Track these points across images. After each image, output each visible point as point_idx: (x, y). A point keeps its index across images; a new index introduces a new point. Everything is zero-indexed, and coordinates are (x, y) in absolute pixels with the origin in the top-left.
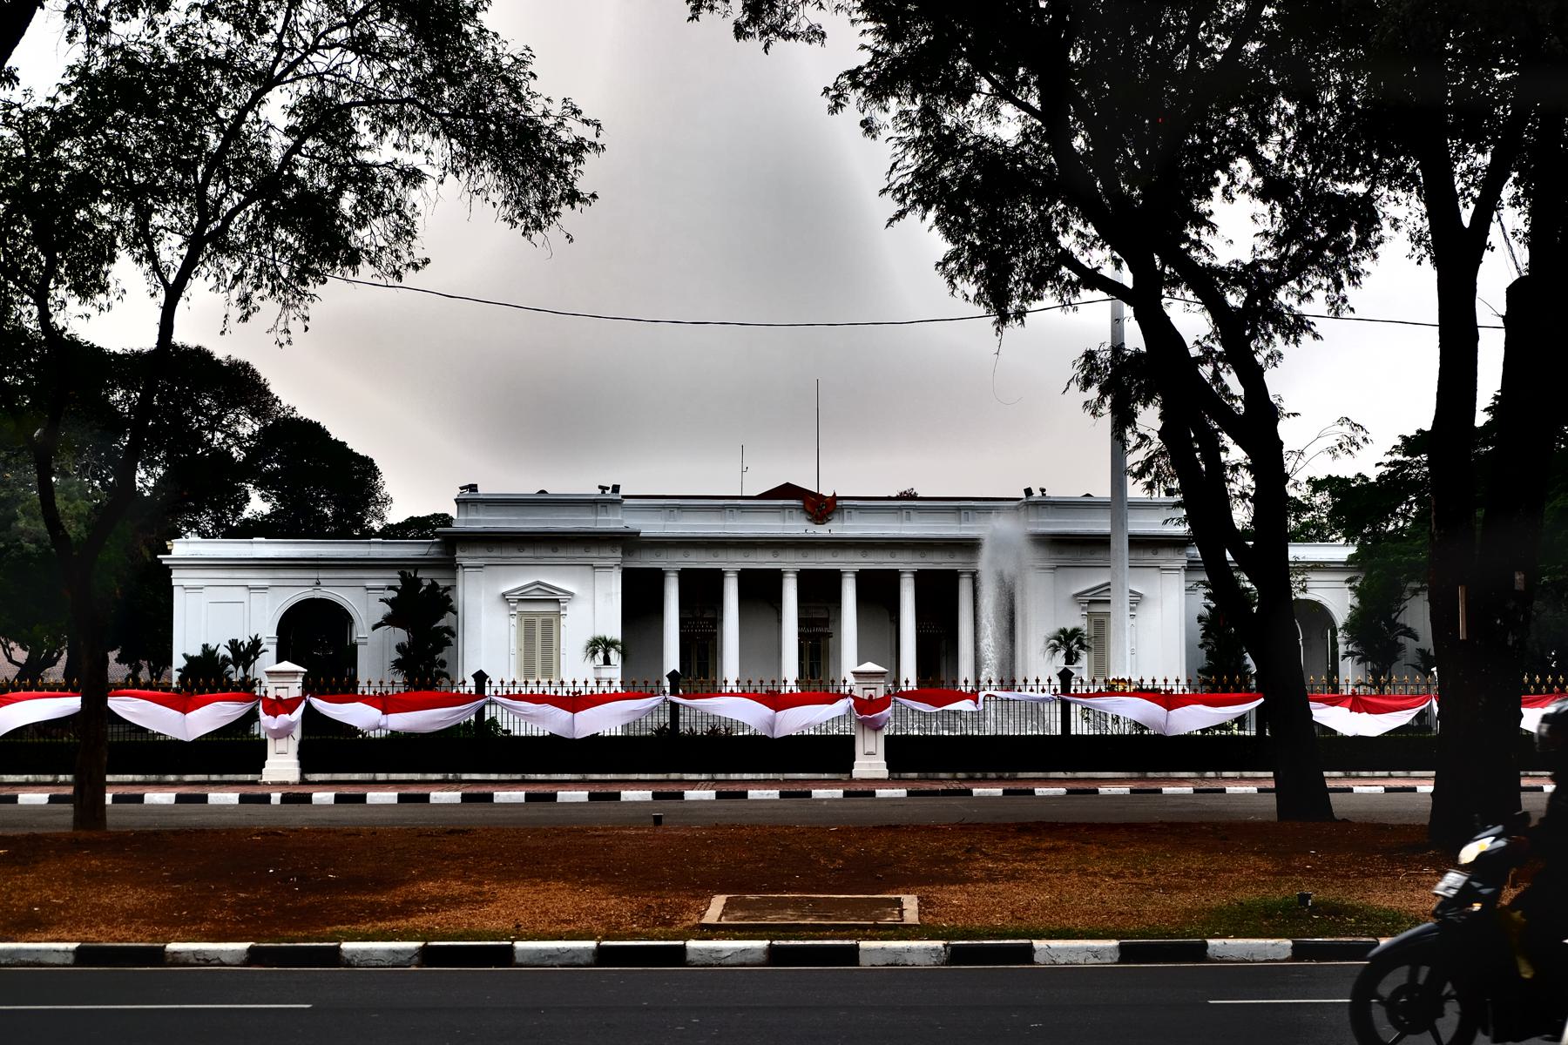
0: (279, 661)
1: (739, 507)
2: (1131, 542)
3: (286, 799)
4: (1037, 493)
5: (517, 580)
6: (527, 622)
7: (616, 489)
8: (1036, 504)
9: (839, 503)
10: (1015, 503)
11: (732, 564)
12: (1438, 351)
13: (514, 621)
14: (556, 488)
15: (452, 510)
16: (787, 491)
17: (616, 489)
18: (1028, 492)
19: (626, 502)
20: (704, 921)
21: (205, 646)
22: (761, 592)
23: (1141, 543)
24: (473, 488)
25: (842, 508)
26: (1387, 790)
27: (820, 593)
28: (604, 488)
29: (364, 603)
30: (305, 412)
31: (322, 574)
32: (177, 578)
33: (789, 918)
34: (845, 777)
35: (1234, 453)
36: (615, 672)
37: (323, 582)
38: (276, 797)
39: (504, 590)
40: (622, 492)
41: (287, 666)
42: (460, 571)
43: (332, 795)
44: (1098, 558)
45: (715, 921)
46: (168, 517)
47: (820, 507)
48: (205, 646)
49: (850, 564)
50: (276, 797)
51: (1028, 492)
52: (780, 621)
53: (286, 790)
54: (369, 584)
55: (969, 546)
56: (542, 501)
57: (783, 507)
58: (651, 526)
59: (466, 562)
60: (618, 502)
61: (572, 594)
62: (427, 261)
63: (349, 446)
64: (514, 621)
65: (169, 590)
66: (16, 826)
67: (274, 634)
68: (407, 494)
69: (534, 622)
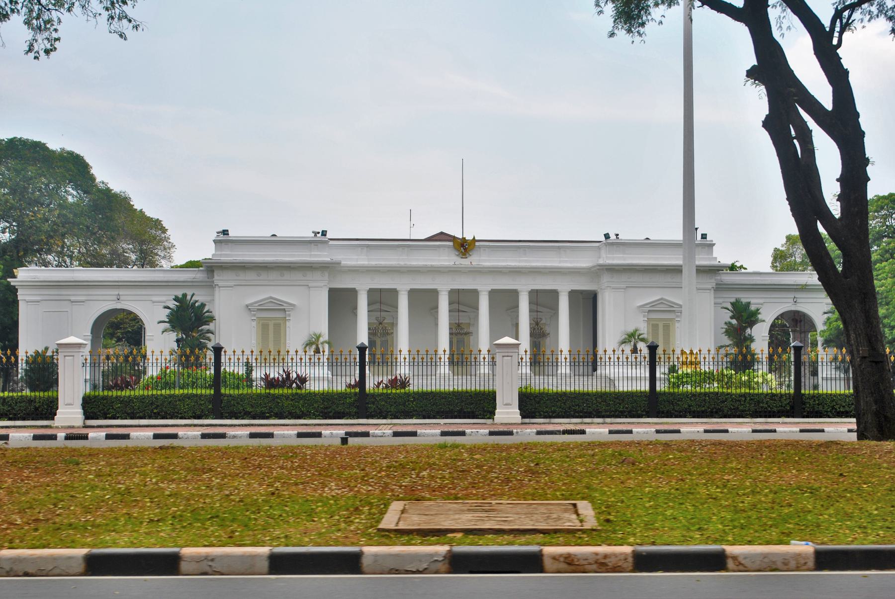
1: (409, 246)
2: (681, 271)
4: (613, 237)
5: (257, 295)
6: (263, 325)
7: (324, 233)
8: (612, 244)
9: (477, 244)
10: (597, 244)
11: (403, 286)
12: (793, 219)
13: (254, 324)
14: (283, 233)
16: (441, 237)
17: (324, 233)
18: (607, 236)
19: (331, 242)
20: (381, 526)
22: (425, 301)
24: (225, 232)
25: (479, 247)
28: (316, 233)
29: (153, 315)
30: (116, 187)
31: (122, 292)
32: (21, 295)
33: (467, 520)
34: (489, 421)
37: (122, 298)
40: (329, 236)
42: (217, 288)
43: (104, 434)
45: (392, 526)
46: (20, 252)
47: (464, 246)
49: (484, 287)
50: (61, 435)
51: (607, 236)
52: (437, 324)
53: (69, 431)
54: (155, 299)
56: (274, 242)
57: (439, 246)
58: (350, 259)
59: (220, 284)
60: (325, 242)
61: (294, 305)
64: (254, 324)
65: (16, 302)
67: (89, 334)
68: (189, 244)
69: (268, 325)
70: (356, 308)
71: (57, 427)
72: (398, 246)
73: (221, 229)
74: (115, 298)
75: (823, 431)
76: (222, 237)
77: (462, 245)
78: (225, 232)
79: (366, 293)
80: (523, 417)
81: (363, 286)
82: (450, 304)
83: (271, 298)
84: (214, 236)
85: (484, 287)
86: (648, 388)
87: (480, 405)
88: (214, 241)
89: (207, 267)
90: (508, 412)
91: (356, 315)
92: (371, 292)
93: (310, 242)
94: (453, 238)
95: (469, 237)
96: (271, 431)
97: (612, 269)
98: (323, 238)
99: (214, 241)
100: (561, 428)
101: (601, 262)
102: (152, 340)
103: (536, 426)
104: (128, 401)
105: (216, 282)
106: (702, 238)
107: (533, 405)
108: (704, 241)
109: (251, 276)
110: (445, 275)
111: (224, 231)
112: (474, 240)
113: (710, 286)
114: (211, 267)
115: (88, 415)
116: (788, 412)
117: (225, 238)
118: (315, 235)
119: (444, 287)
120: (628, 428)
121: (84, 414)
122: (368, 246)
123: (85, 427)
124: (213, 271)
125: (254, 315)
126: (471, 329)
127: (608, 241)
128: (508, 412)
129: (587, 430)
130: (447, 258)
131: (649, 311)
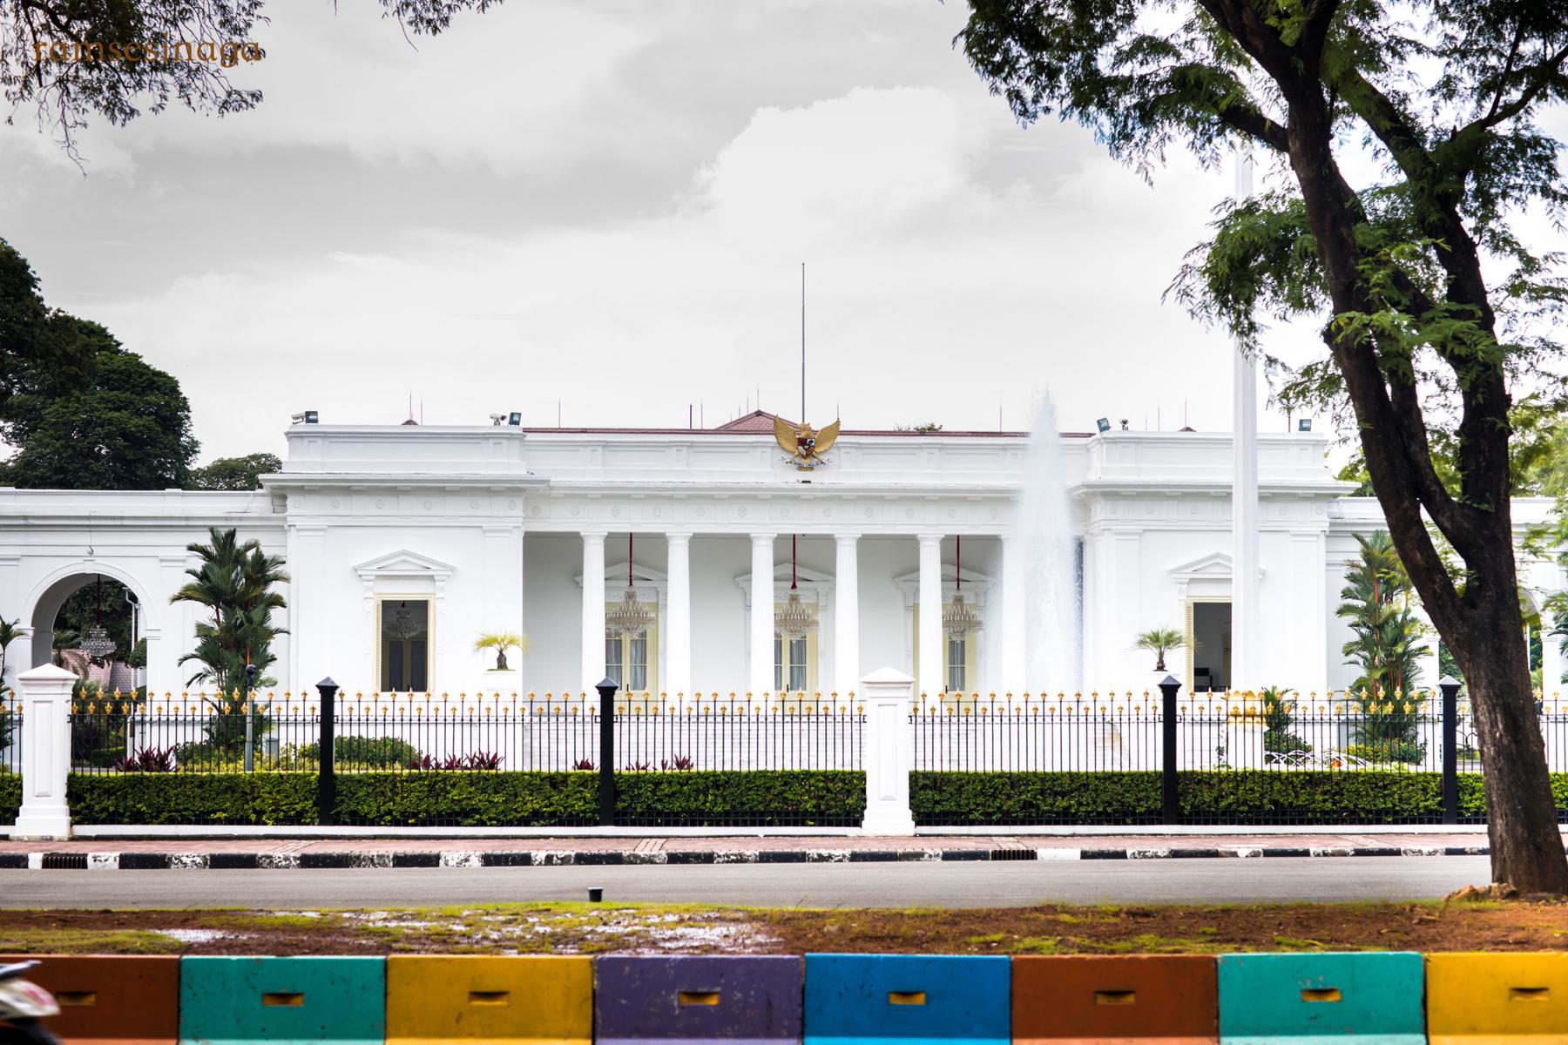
0: (35, 664)
2: (1229, 495)
3: (50, 862)
4: (1116, 427)
8: (1114, 441)
9: (840, 439)
11: (678, 529)
15: (280, 449)
18: (1103, 426)
19: (530, 437)
21: (273, 659)
23: (1271, 496)
24: (310, 417)
26: (1085, 855)
27: (802, 561)
35: (1427, 360)
36: (512, 681)
37: (97, 551)
38: (35, 860)
39: (356, 563)
40: (523, 424)
41: (49, 670)
44: (1209, 513)
47: (806, 446)
48: (273, 659)
49: (847, 530)
50: (35, 860)
51: (1103, 426)
55: (1001, 499)
56: (410, 434)
57: (753, 445)
59: (300, 523)
61: (453, 569)
62: (257, 96)
63: (145, 360)
66: (164, 902)
70: (579, 572)
71: (20, 840)
72: (669, 445)
73: (302, 412)
74: (85, 551)
75: (1031, 855)
76: (303, 427)
77: (802, 442)
78: (310, 417)
79: (686, 542)
80: (918, 823)
81: (594, 529)
82: (776, 564)
83: (404, 553)
84: (287, 424)
85: (847, 530)
86: (1160, 768)
87: (839, 799)
88: (287, 434)
89: (273, 488)
90: (888, 814)
91: (579, 586)
92: (611, 539)
93: (486, 437)
94: (778, 427)
95: (818, 423)
96: (435, 851)
97: (1114, 494)
98: (514, 429)
99: (287, 434)
100: (990, 847)
101: (1093, 477)
102: (158, 639)
103: (941, 840)
104: (231, 785)
105: (290, 520)
106: (1302, 429)
107: (937, 798)
108: (1305, 435)
109: (1167, 513)
110: (762, 500)
111: (308, 414)
112: (834, 430)
113: (1318, 530)
114: (282, 488)
115: (922, 818)
116: (1159, 813)
117: (311, 428)
118: (497, 423)
119: (763, 531)
120: (518, 848)
121: (72, 813)
122: (606, 445)
123: (74, 839)
124: (284, 498)
125: (368, 589)
126: (820, 617)
127: (1106, 434)
128: (888, 814)
129: (1040, 852)
130: (766, 467)
131: (1192, 581)
